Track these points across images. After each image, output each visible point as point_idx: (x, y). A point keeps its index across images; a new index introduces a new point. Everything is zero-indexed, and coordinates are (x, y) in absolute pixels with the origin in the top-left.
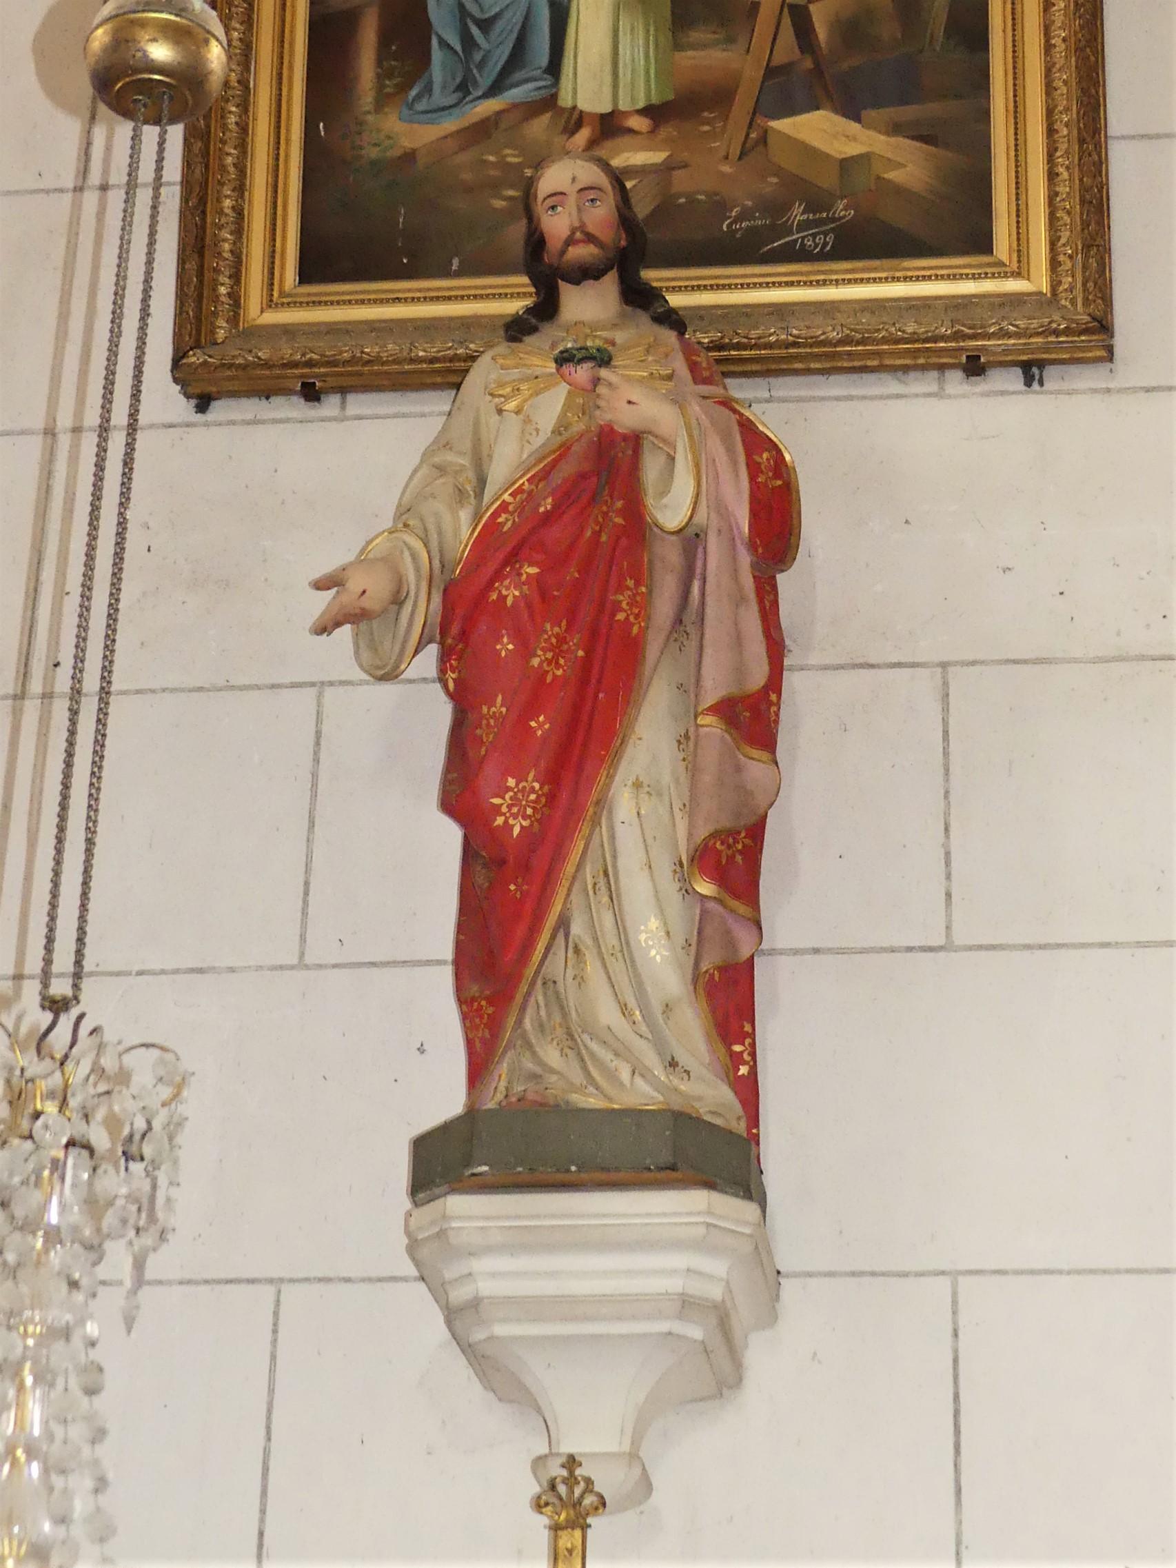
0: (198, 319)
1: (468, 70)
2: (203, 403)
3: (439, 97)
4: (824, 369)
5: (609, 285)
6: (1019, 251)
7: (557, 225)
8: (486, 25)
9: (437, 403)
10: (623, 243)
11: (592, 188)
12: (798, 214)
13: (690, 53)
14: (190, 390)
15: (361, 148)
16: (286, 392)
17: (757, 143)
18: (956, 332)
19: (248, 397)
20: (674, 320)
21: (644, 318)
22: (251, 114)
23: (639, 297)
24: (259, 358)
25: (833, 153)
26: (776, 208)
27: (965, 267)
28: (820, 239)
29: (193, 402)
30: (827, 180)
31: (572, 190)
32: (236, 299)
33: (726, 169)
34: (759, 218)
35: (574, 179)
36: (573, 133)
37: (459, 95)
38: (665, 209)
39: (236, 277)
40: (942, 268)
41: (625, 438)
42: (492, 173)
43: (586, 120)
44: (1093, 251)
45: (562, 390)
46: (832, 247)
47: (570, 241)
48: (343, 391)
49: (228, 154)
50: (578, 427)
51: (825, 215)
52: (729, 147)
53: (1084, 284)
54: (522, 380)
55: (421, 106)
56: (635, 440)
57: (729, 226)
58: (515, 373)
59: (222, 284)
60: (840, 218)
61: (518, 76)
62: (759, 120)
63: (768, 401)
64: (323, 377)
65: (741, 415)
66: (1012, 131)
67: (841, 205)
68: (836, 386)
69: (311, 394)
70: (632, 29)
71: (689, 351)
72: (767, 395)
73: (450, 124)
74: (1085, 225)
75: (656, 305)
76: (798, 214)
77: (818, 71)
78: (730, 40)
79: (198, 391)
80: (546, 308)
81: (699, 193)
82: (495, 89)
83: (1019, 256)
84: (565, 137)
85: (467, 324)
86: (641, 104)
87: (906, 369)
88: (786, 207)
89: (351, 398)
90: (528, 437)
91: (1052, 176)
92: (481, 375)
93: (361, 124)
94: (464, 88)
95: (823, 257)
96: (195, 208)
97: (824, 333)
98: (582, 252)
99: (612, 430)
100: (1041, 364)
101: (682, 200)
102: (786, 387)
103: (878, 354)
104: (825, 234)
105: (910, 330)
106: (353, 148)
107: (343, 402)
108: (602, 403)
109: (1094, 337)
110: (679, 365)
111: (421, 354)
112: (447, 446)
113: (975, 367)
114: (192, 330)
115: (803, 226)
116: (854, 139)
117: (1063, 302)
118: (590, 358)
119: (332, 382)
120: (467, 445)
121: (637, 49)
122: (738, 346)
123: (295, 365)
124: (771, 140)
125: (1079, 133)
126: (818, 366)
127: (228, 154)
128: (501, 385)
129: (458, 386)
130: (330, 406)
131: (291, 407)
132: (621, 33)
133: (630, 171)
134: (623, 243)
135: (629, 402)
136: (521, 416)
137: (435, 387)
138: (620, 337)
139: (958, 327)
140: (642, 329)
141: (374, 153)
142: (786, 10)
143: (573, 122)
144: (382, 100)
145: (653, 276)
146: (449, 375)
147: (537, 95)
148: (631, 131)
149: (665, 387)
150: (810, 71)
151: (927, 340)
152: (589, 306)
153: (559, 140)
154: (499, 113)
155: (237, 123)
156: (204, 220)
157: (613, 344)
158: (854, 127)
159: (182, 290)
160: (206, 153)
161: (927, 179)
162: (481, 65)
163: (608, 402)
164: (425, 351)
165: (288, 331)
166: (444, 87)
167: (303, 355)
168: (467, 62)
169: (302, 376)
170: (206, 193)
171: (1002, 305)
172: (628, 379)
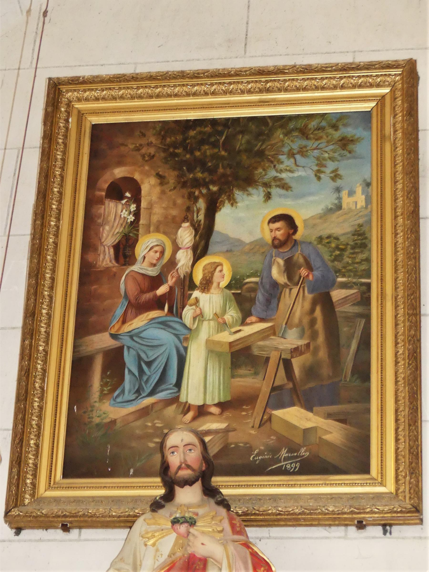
0: (17, 494)
1: (140, 385)
2: (18, 531)
3: (127, 396)
4: (293, 525)
5: (198, 486)
6: (382, 473)
7: (174, 460)
8: (149, 364)
9: (120, 534)
10: (204, 468)
11: (189, 444)
12: (284, 453)
13: (238, 379)
14: (13, 526)
15: (92, 418)
16: (55, 528)
17: (266, 421)
18: (352, 511)
19: (38, 529)
20: (224, 503)
21: (212, 501)
22: (44, 401)
23: (210, 492)
24: (43, 513)
25: (301, 427)
26: (275, 451)
27: (357, 479)
28: (293, 465)
29: (14, 531)
30: (298, 440)
31: (181, 445)
32: (34, 485)
33: (253, 432)
34: (267, 455)
35: (182, 440)
36: (185, 414)
37: (136, 395)
38: (225, 450)
39: (35, 475)
40: (347, 480)
41: (200, 559)
42: (149, 431)
43: (191, 407)
44: (414, 475)
45: (174, 536)
46: (299, 468)
47: (179, 468)
48: (80, 528)
49: (33, 420)
50: (179, 554)
51: (296, 454)
52: (254, 421)
53: (410, 490)
54: (156, 531)
55: (119, 400)
56: (204, 561)
57: (254, 458)
58: (154, 527)
59: (29, 479)
60: (304, 456)
61: (163, 387)
62: (268, 410)
63: (268, 538)
64: (71, 522)
65: (253, 549)
66: (380, 419)
67: (303, 450)
68: (300, 531)
69: (66, 528)
70: (213, 368)
71: (231, 519)
72: (268, 536)
73: (132, 408)
74: (411, 463)
75: (218, 496)
76: (284, 453)
77: (294, 390)
78: (256, 374)
79: (15, 526)
80: (169, 496)
81: (241, 443)
82: (152, 393)
83: (382, 476)
84: (182, 415)
85: (136, 499)
86: (216, 401)
87: (330, 525)
88: (279, 450)
89: (84, 531)
90: (157, 558)
91: (397, 440)
92: (140, 525)
93: (93, 407)
94: (138, 392)
95: (294, 473)
96: (18, 443)
97: (293, 510)
98: (185, 473)
99: (194, 555)
100: (391, 525)
101: (233, 446)
102: (275, 531)
103: (319, 520)
104: (296, 463)
105: (331, 510)
106: (89, 418)
107: (80, 532)
108: (190, 544)
109: (414, 515)
110: (226, 525)
111: (114, 514)
112: (122, 560)
113: (361, 525)
114: (14, 499)
115: (286, 459)
116: (308, 420)
117: (400, 497)
118: (186, 522)
119: (75, 524)
120: (131, 561)
121: (215, 376)
122: (255, 514)
123: (59, 516)
124: (273, 419)
125: (409, 421)
126: (291, 523)
127: (33, 420)
128: (147, 533)
129: (131, 528)
130: (75, 532)
131: (57, 534)
132: (208, 369)
133: (208, 432)
134: (204, 468)
135: (203, 544)
136: (155, 548)
137: (120, 527)
138: (201, 511)
139: (352, 509)
140: (210, 508)
141: (97, 420)
142: (281, 360)
143: (186, 409)
144: (103, 396)
145: (216, 480)
146: (128, 522)
147: (170, 397)
148: (211, 414)
149: (219, 536)
150: (291, 389)
151: (338, 514)
152: (188, 496)
153: (180, 417)
154: (153, 405)
155: (38, 406)
156: (21, 450)
157: (197, 514)
158: (310, 415)
159: (10, 481)
160: (23, 419)
161: (342, 440)
162: (147, 382)
163: (193, 543)
164: (115, 512)
165: (57, 500)
166: (129, 392)
167: (62, 513)
168: (140, 380)
169: (62, 521)
170: (23, 438)
171: (373, 498)
172: (203, 533)
